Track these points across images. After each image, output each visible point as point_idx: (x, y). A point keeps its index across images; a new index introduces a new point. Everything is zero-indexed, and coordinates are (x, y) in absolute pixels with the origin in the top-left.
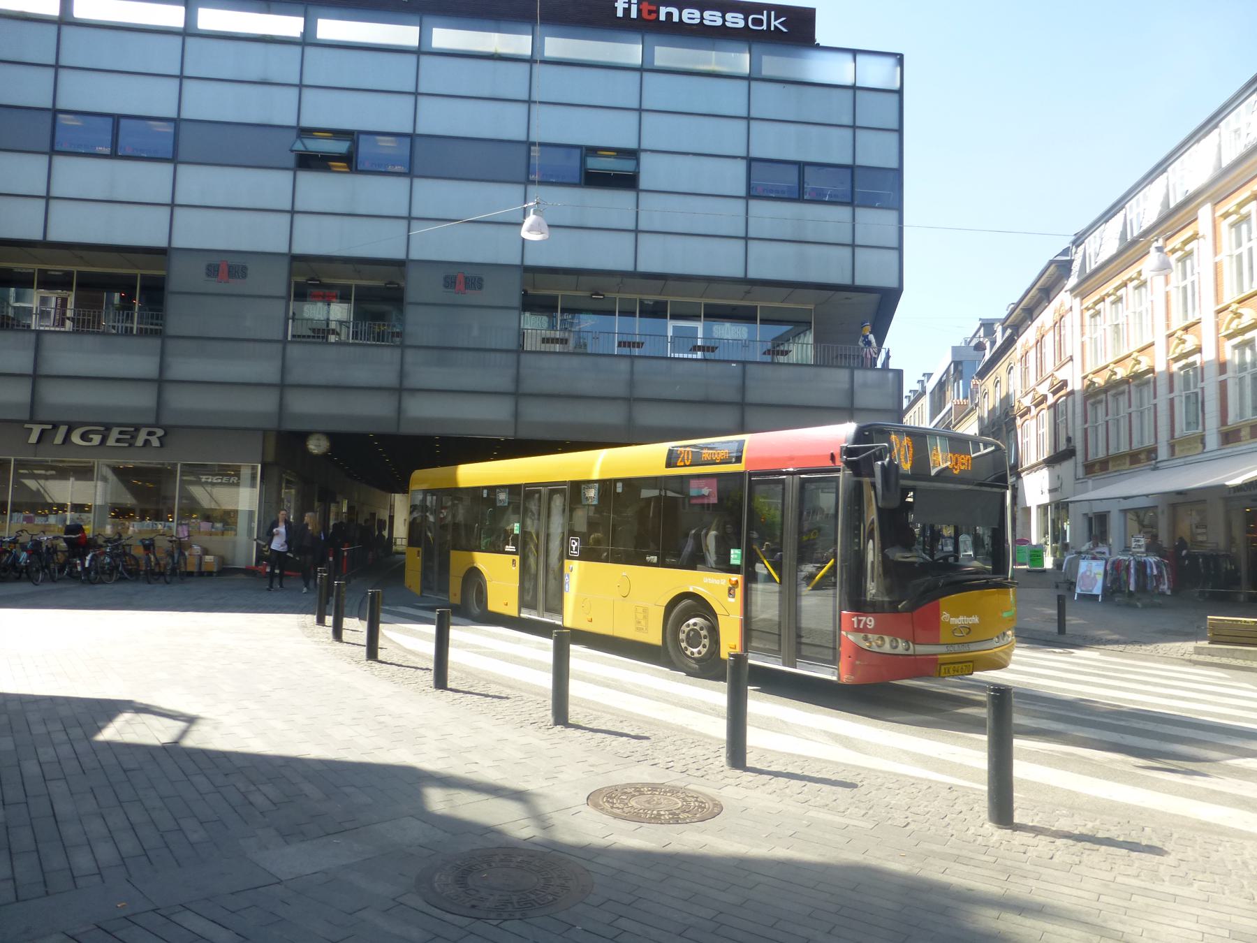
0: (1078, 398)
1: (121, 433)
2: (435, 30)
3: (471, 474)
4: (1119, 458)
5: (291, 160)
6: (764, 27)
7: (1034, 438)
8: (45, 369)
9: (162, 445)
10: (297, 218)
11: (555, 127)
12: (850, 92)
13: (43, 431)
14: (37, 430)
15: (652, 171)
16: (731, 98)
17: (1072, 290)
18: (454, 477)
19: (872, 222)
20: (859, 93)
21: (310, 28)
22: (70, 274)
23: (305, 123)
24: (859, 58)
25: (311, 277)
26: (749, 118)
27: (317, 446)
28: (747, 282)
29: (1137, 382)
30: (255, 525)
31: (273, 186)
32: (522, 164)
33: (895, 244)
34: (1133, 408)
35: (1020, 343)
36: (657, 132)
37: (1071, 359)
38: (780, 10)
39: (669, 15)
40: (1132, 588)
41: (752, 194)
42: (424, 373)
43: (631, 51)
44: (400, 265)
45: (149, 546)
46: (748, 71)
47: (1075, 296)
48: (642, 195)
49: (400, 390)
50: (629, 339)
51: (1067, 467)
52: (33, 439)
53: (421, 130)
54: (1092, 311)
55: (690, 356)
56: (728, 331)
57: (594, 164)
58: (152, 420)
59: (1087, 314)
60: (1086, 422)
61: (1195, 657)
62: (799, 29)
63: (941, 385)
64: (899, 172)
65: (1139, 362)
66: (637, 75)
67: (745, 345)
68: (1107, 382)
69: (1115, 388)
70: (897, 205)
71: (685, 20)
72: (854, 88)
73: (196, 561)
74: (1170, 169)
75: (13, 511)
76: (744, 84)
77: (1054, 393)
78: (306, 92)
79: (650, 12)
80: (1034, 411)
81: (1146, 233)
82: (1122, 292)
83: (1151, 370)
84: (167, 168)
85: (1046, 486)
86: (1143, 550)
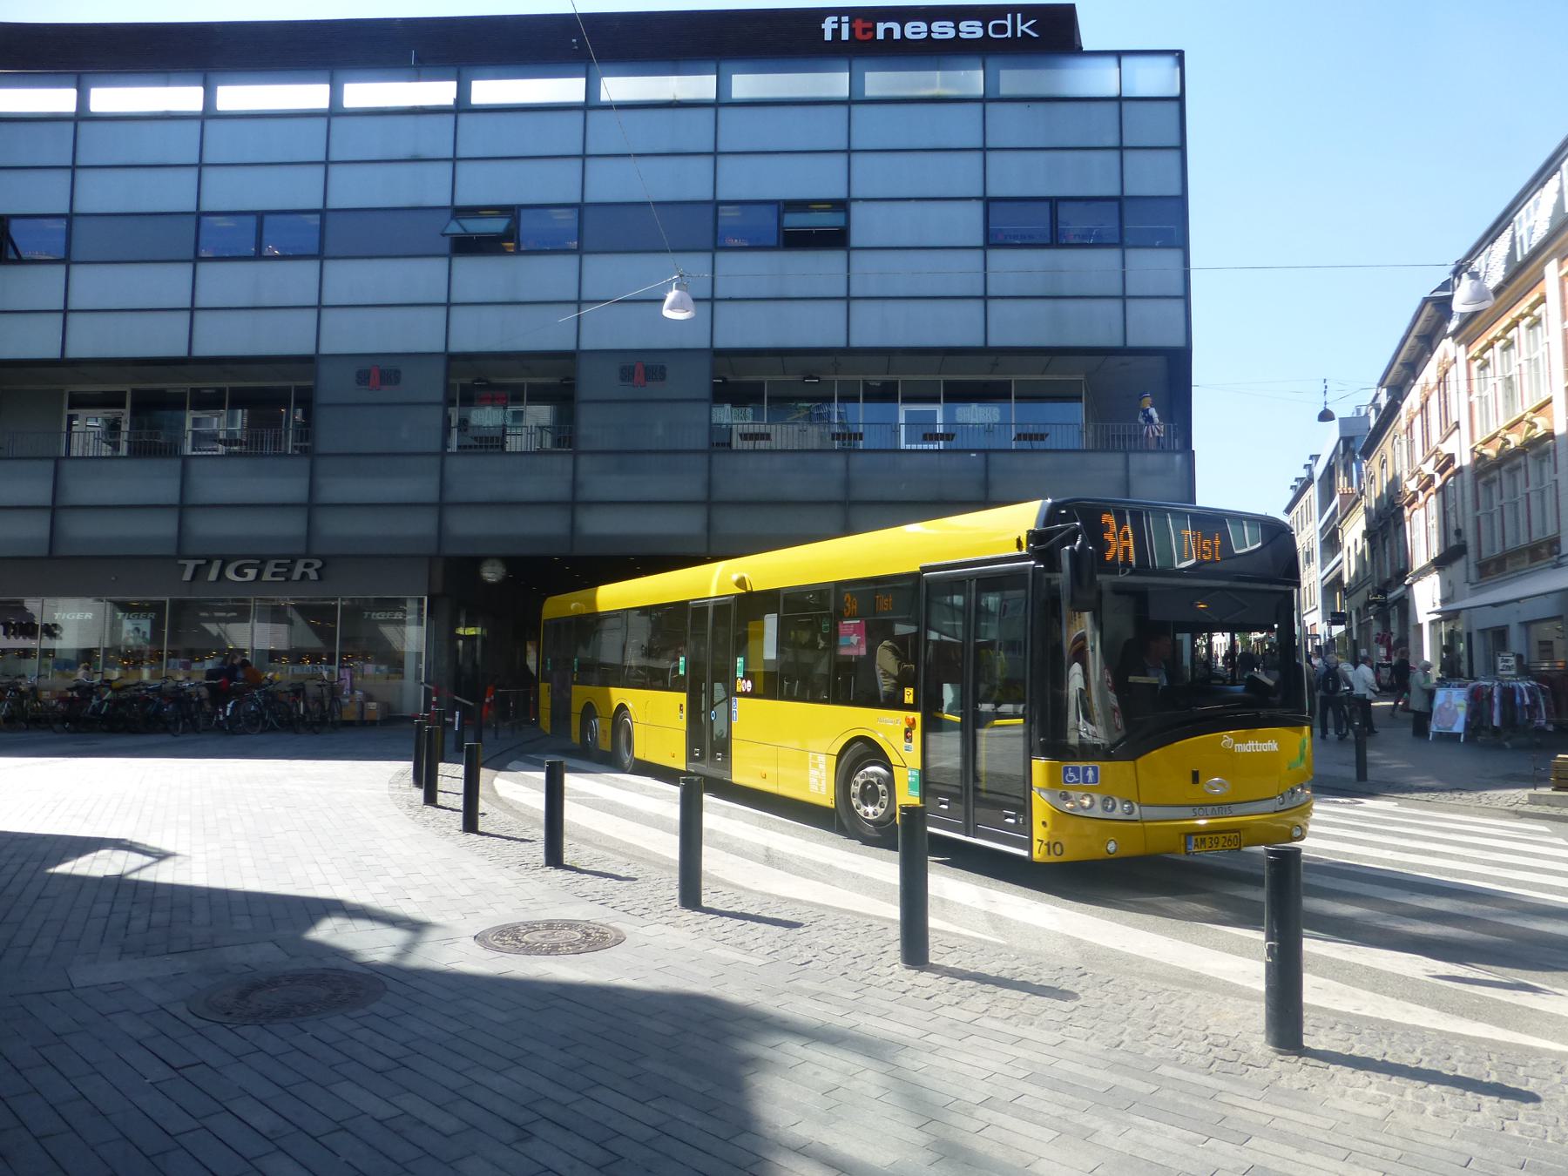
0: (1467, 476)
1: (277, 566)
2: (868, 75)
3: (613, 596)
4: (1517, 553)
5: (446, 245)
6: (1009, 34)
7: (1423, 535)
8: (193, 498)
9: (320, 578)
10: (854, 305)
11: (746, 181)
12: (1115, 105)
13: (197, 567)
14: (191, 565)
15: (866, 224)
16: (962, 126)
17: (1455, 334)
18: (593, 602)
19: (1148, 266)
20: (1125, 105)
21: (463, 93)
22: (221, 391)
23: (461, 201)
24: (1126, 61)
25: (476, 378)
26: (984, 150)
27: (491, 574)
28: (985, 351)
29: (1533, 452)
30: (423, 667)
31: (424, 276)
32: (705, 227)
33: (1180, 292)
34: (1532, 487)
35: (1405, 406)
36: (872, 176)
37: (1457, 425)
38: (1028, 11)
39: (889, 31)
40: (1496, 722)
41: (992, 241)
42: (601, 483)
43: (835, 83)
44: (308, 362)
45: (298, 691)
46: (981, 92)
47: (1459, 343)
48: (854, 254)
49: (573, 504)
50: (1031, 429)
51: (1458, 567)
52: (187, 576)
53: (589, 199)
54: (1479, 362)
55: (925, 447)
56: (975, 414)
57: (794, 221)
58: (301, 550)
59: (1475, 365)
60: (1478, 508)
61: (1527, 808)
62: (1056, 34)
63: (1330, 471)
64: (1181, 200)
65: (1534, 426)
66: (843, 109)
67: (988, 429)
68: (1499, 452)
69: (1509, 461)
70: (1181, 242)
71: (908, 35)
72: (1120, 99)
73: (356, 708)
74: (1564, 166)
75: (169, 657)
76: (978, 107)
77: (1441, 472)
78: (722, 160)
79: (865, 31)
80: (1421, 498)
81: (1536, 253)
82: (1513, 333)
83: (1550, 435)
84: (313, 266)
85: (1438, 597)
86: (1513, 672)
